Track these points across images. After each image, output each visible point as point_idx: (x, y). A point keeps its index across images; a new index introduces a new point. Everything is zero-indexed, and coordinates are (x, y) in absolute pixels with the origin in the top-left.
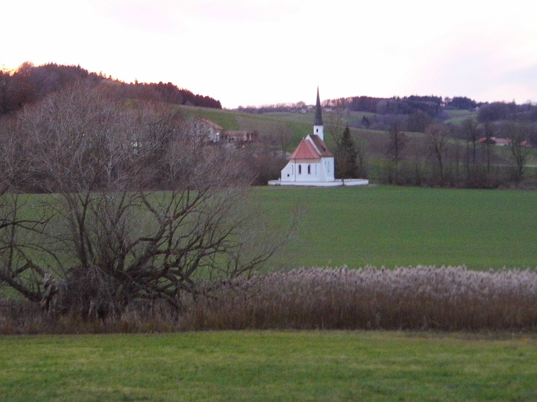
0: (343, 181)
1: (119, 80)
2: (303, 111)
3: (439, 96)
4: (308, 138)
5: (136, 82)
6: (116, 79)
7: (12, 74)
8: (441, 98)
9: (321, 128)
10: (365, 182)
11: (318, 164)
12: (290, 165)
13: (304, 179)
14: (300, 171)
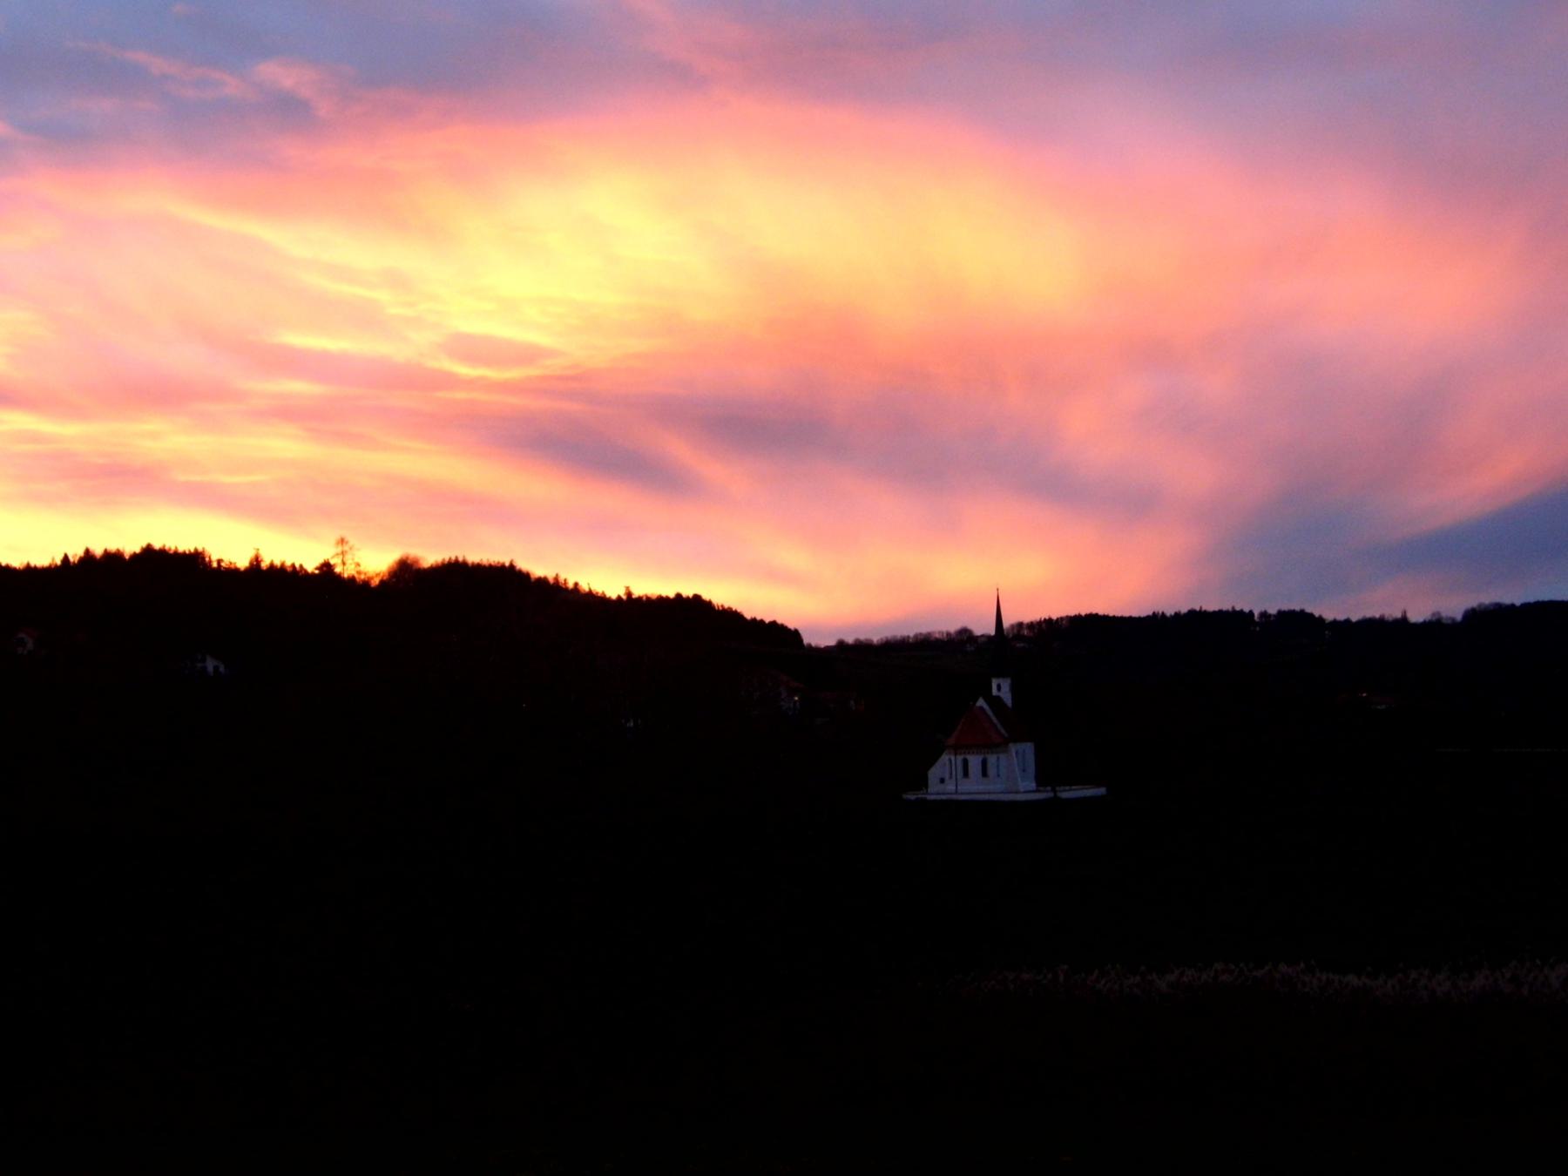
0: (1054, 790)
1: (32, 564)
2: (970, 648)
3: (1246, 610)
4: (981, 702)
5: (629, 594)
6: (81, 553)
7: (375, 582)
8: (1251, 613)
9: (1006, 684)
10: (1102, 791)
11: (1002, 756)
12: (945, 758)
13: (974, 788)
14: (966, 774)
